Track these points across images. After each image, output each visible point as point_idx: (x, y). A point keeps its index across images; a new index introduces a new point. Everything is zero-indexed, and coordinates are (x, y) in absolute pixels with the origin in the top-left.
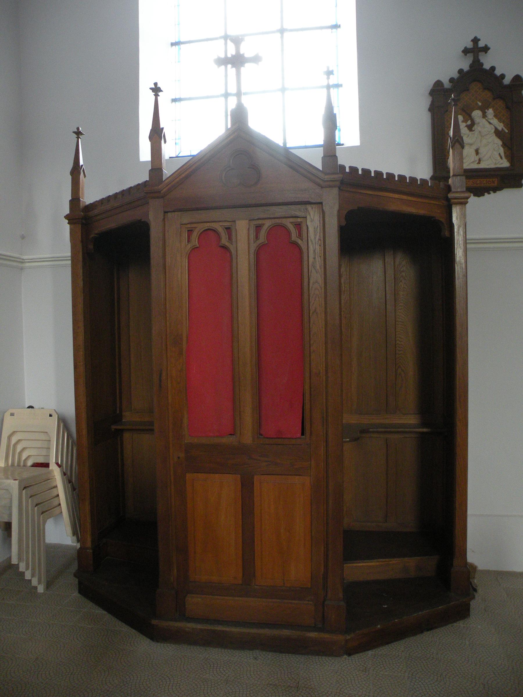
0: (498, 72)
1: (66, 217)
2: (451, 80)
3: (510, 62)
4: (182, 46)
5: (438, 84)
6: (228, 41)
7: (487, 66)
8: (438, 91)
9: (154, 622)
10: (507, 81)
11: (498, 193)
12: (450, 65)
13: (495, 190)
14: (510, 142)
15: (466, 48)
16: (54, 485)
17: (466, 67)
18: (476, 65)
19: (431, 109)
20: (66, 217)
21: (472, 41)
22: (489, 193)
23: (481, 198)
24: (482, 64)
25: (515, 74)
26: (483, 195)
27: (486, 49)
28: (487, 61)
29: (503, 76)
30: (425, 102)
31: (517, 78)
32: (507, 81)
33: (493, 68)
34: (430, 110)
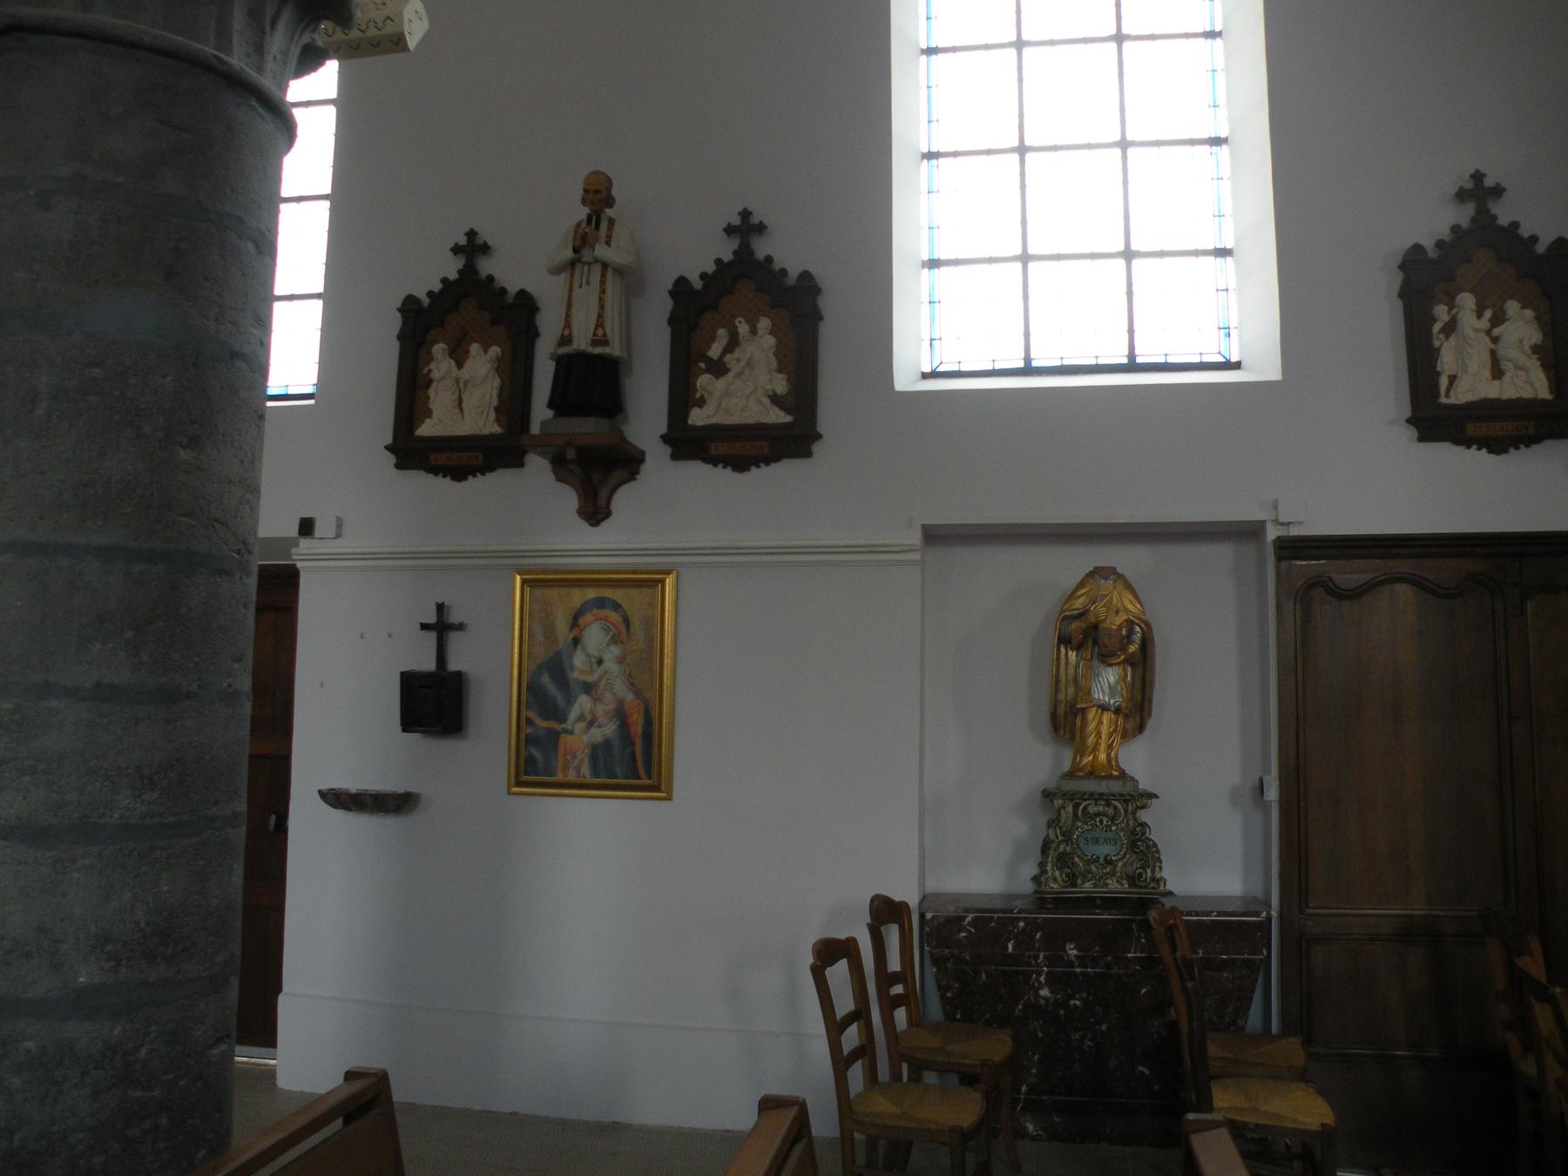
0: (1525, 232)
1: (1409, 421)
2: (1440, 244)
3: (1538, 216)
4: (942, 161)
5: (1417, 249)
7: (1503, 220)
8: (410, 307)
11: (1535, 448)
14: (1552, 356)
15: (1461, 188)
17: (727, 256)
18: (744, 254)
19: (401, 337)
20: (1409, 421)
21: (1472, 176)
22: (1517, 448)
23: (464, 483)
24: (1494, 217)
25: (674, 277)
26: (465, 479)
27: (1498, 191)
29: (1534, 239)
30: (396, 322)
31: (1560, 241)
34: (1401, 295)
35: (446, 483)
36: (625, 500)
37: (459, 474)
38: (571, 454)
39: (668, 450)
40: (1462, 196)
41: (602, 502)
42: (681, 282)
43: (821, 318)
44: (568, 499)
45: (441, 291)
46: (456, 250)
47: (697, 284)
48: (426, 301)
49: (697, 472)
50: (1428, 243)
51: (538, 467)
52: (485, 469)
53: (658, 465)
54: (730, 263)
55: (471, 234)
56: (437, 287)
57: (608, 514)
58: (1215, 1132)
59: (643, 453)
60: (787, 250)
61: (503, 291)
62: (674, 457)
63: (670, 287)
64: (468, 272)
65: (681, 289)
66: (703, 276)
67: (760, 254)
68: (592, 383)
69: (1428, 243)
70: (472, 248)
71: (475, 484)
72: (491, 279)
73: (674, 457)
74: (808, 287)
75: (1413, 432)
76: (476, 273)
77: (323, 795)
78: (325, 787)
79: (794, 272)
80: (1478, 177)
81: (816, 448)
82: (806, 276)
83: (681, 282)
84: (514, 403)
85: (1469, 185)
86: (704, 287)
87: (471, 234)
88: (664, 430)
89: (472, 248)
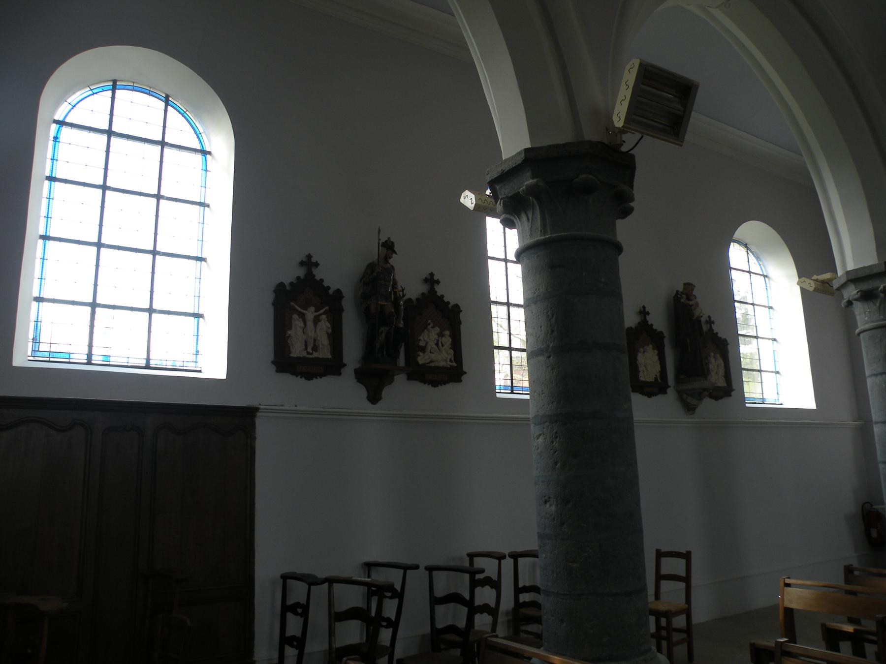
1: (273, 362)
2: (291, 284)
5: (281, 285)
6: (398, 587)
8: (280, 289)
9: (327, 308)
10: (331, 292)
12: (291, 273)
13: (445, 383)
16: (761, 257)
18: (310, 275)
19: (275, 304)
20: (273, 362)
23: (311, 382)
24: (314, 276)
28: (318, 274)
29: (329, 288)
30: (270, 297)
32: (331, 292)
33: (322, 280)
34: (273, 304)
36: (386, 392)
37: (309, 377)
40: (302, 263)
43: (460, 323)
44: (362, 391)
45: (323, 286)
50: (287, 283)
53: (400, 380)
58: (459, 606)
60: (448, 292)
67: (318, 278)
69: (287, 282)
70: (309, 263)
71: (317, 382)
74: (457, 309)
75: (273, 368)
79: (452, 303)
80: (309, 257)
81: (464, 378)
82: (457, 306)
84: (336, 338)
85: (429, 277)
89: (309, 263)
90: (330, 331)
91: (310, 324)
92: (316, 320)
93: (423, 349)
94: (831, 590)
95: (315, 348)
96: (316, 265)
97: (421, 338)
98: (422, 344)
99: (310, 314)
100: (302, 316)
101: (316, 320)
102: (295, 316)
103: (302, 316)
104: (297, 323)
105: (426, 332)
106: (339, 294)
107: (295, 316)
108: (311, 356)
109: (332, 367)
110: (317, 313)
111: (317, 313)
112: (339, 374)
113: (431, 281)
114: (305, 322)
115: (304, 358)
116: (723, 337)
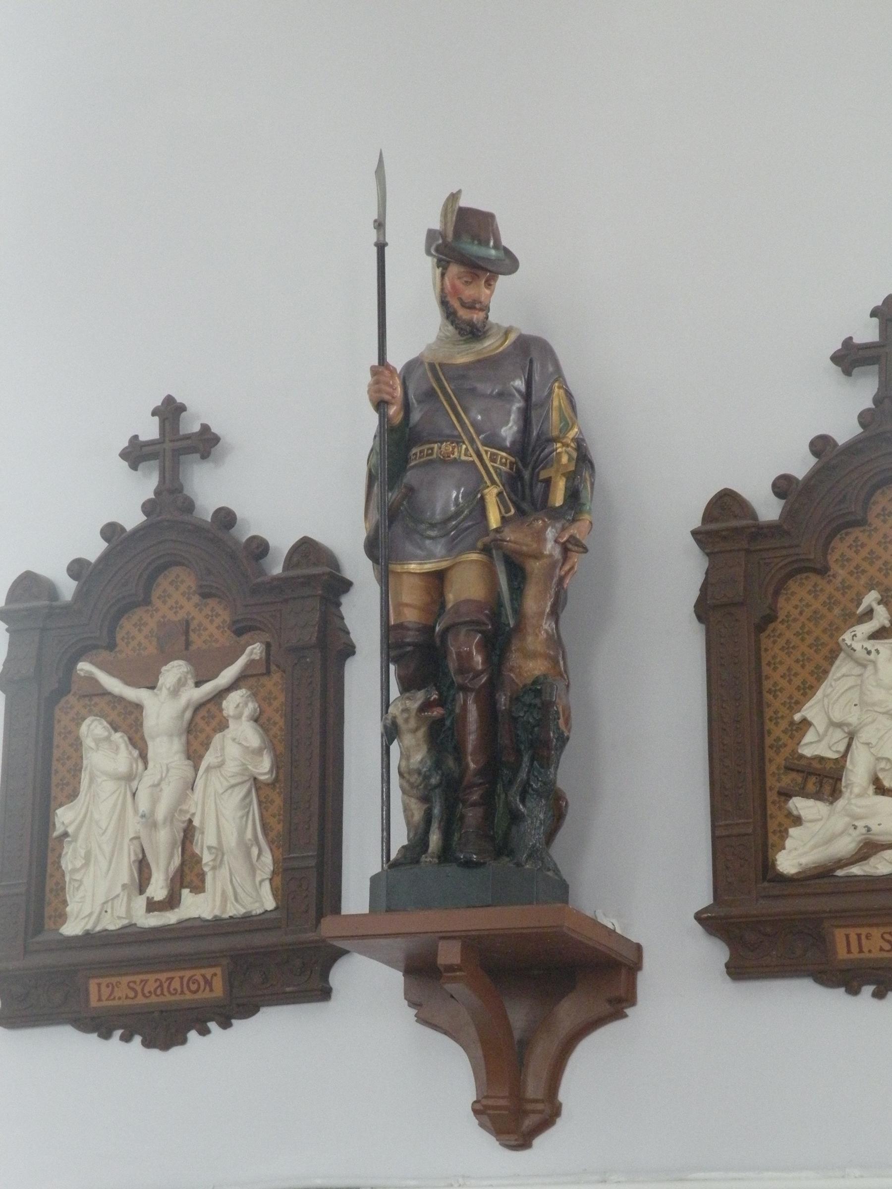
20: (708, 921)
35: (127, 1056)
36: (596, 1071)
37: (164, 1028)
38: (449, 954)
39: (717, 953)
40: (136, 454)
41: (533, 1088)
42: (726, 504)
44: (450, 1073)
46: (136, 454)
47: (769, 509)
48: (68, 588)
49: (799, 1009)
51: (369, 985)
52: (230, 1010)
54: (854, 447)
55: (170, 411)
56: (94, 548)
57: (550, 1114)
59: (639, 948)
61: (259, 548)
62: (738, 970)
63: (696, 522)
64: (170, 506)
65: (724, 524)
66: (783, 486)
68: (499, 757)
70: (175, 444)
72: (226, 518)
73: (738, 970)
76: (189, 506)
77: (459, 192)
78: (463, 193)
83: (726, 504)
84: (303, 807)
86: (788, 514)
87: (170, 411)
88: (703, 897)
89: (175, 444)
90: (264, 767)
91: (165, 750)
92: (200, 728)
93: (826, 780)
94: (376, 489)
95: (189, 875)
96: (206, 443)
97: (811, 711)
98: (816, 745)
99: (164, 705)
100: (128, 721)
101: (200, 728)
102: (93, 729)
103: (128, 721)
104: (102, 752)
105: (841, 668)
106: (316, 575)
107: (93, 729)
108: (171, 918)
109: (272, 964)
110: (208, 688)
111: (208, 688)
112: (325, 994)
113: (849, 358)
114: (139, 744)
115: (130, 936)
116: (572, 1088)
